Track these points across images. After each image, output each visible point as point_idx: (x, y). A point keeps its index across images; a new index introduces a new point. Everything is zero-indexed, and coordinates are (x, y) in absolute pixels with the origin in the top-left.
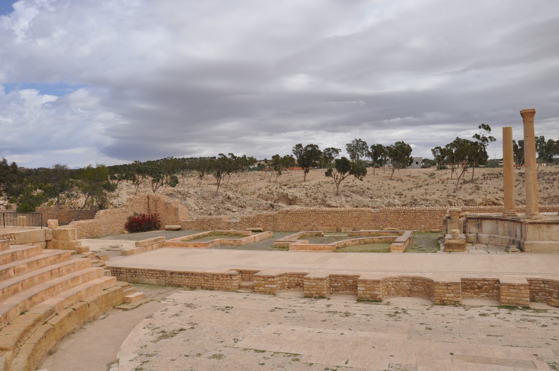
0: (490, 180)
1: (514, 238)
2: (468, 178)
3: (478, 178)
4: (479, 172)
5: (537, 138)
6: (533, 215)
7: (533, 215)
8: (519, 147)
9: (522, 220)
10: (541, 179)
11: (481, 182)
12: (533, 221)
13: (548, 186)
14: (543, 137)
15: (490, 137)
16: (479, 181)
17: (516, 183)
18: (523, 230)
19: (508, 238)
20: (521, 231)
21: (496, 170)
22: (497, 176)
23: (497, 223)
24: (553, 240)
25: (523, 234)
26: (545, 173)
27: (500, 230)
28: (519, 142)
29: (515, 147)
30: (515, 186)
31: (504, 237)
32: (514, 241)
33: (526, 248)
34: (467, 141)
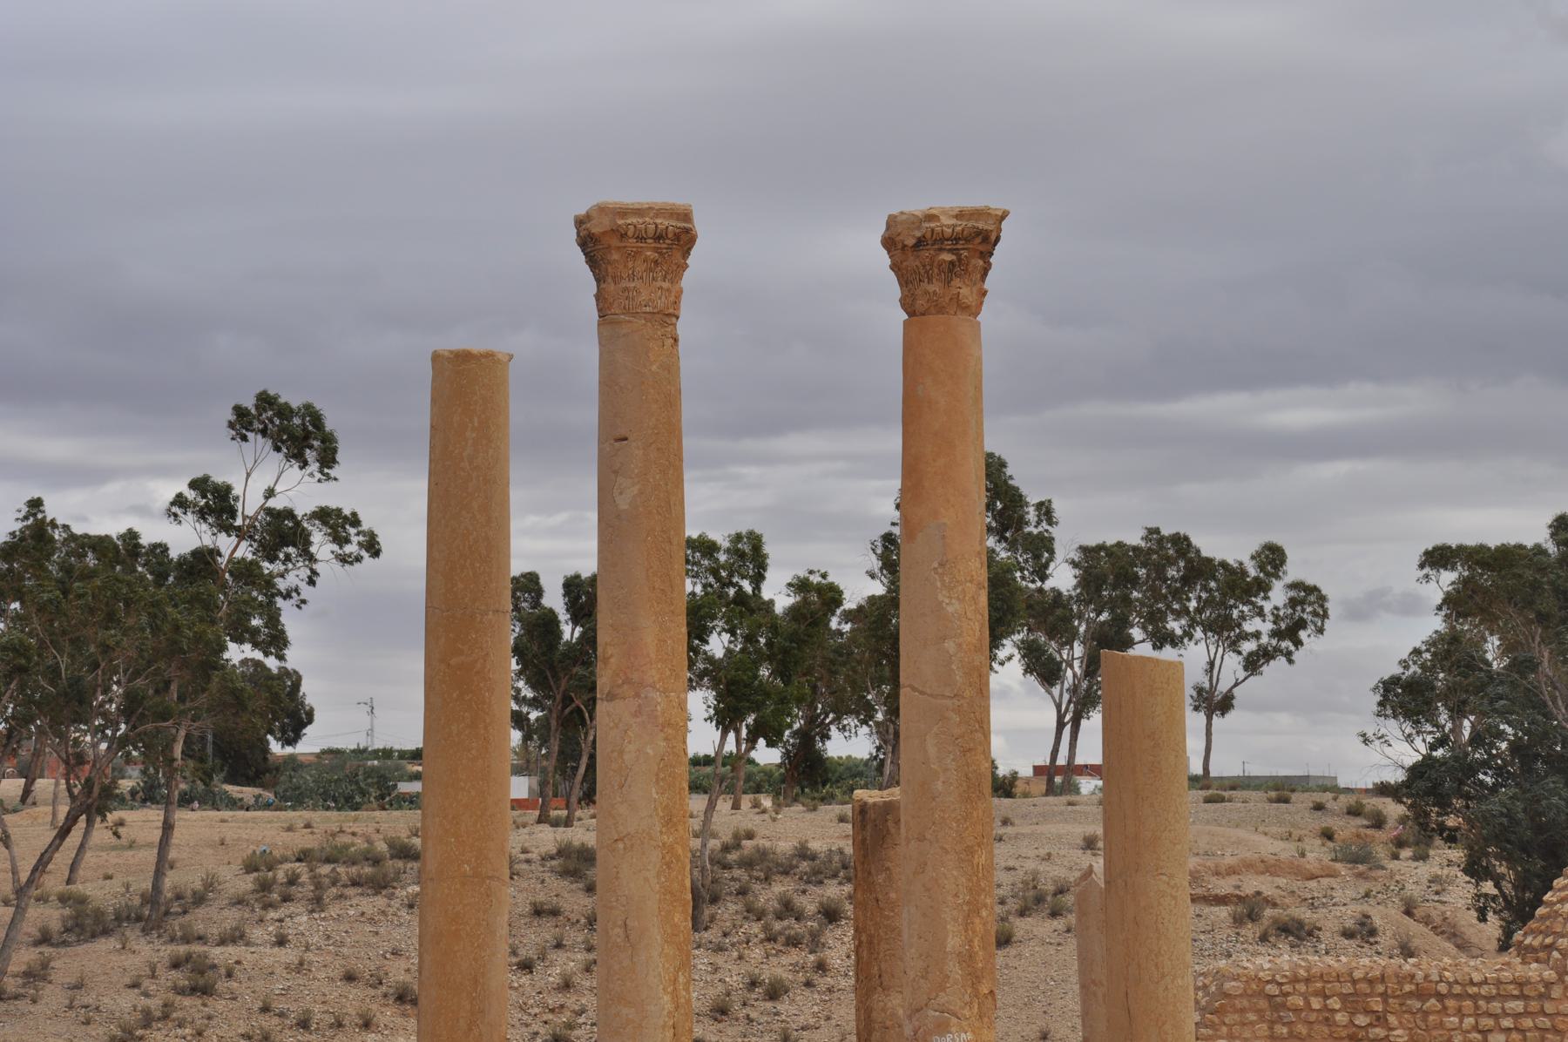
0: (317, 903)
2: (116, 886)
3: (210, 884)
4: (220, 838)
5: (706, 547)
8: (569, 632)
10: (729, 910)
11: (231, 917)
13: (780, 967)
14: (756, 541)
15: (324, 515)
16: (215, 918)
17: (534, 937)
26: (763, 854)
28: (573, 586)
30: (526, 966)
34: (126, 550)
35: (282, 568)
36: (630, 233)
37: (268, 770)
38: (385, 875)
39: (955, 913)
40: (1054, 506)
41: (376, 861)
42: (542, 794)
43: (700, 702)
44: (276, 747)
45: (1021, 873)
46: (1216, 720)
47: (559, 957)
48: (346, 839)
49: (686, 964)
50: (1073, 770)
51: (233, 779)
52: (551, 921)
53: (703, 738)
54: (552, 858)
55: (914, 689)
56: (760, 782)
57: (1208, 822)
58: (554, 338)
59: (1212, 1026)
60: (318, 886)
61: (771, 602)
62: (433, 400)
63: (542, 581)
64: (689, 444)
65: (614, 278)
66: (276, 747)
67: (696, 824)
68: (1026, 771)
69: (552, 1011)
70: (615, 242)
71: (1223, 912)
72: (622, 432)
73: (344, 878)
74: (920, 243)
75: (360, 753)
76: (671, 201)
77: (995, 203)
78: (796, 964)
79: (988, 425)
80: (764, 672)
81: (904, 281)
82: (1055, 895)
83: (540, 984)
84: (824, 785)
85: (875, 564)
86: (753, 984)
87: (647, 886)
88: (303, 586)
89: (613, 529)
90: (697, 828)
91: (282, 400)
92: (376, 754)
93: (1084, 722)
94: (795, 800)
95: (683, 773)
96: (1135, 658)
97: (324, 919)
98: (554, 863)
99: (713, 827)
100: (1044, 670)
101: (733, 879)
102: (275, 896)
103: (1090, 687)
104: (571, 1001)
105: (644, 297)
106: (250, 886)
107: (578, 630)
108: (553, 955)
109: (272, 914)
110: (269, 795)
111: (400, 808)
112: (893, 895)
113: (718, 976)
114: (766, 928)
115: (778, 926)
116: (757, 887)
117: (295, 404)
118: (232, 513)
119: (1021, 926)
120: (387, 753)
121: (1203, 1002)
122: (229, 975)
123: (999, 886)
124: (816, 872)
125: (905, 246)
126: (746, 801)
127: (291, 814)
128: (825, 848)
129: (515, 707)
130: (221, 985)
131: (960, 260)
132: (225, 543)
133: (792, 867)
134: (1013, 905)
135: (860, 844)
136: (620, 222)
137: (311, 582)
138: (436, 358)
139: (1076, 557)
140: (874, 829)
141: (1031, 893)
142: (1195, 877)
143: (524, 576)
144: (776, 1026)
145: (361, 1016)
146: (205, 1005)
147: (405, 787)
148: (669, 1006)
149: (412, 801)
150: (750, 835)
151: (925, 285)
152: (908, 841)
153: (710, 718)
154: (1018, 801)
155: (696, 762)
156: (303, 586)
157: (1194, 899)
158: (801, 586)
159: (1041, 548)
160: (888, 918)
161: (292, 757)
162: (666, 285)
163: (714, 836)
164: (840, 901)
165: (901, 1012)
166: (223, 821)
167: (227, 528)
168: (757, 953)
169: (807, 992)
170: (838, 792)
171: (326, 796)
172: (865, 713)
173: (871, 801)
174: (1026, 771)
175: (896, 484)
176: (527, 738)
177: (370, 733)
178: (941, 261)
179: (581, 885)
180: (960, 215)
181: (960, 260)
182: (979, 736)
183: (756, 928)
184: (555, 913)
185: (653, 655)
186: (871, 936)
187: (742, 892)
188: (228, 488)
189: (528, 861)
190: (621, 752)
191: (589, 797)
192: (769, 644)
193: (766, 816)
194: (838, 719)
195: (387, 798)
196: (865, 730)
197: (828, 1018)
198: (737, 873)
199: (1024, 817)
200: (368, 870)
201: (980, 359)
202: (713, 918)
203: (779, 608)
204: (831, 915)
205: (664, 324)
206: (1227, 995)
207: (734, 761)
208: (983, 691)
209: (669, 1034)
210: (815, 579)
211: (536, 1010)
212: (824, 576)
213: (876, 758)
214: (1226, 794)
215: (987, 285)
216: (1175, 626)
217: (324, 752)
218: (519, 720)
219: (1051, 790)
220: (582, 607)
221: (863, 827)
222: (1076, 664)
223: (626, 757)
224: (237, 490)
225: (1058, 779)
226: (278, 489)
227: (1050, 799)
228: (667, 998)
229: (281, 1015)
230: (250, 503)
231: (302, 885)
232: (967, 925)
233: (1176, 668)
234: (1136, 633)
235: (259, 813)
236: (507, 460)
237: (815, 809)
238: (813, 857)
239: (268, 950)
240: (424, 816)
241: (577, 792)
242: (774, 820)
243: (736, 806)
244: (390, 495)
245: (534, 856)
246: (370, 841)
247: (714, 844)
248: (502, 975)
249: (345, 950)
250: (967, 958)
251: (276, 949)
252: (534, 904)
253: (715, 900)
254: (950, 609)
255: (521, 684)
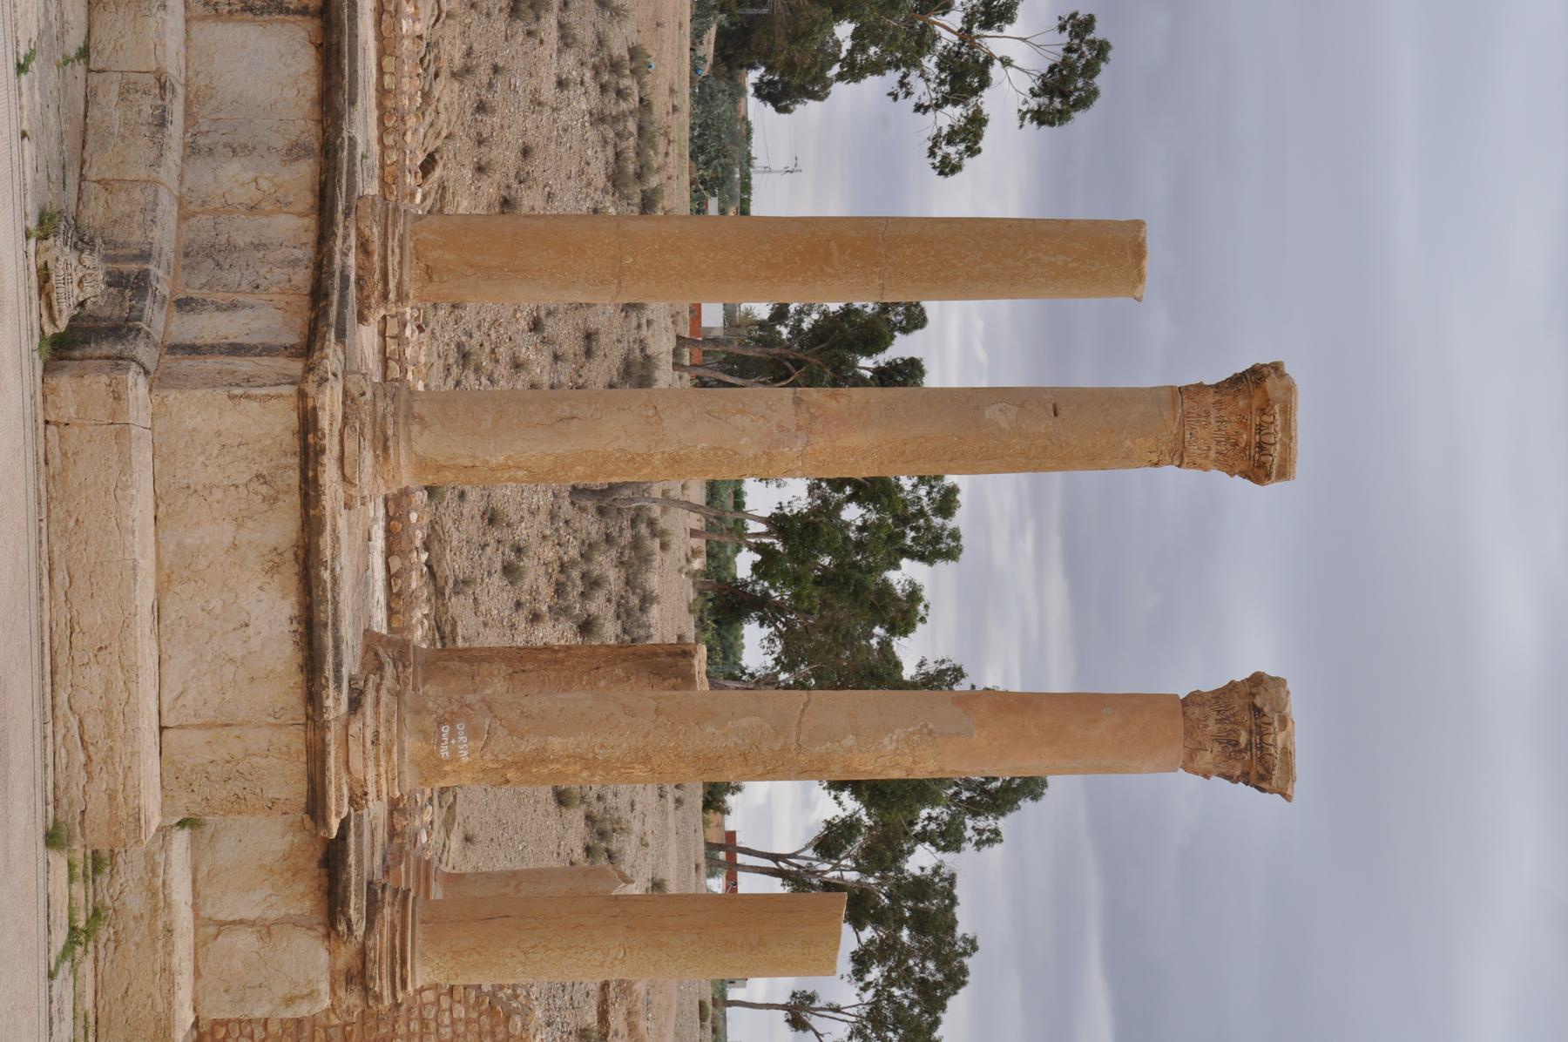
0: (599, 119)
1: (164, 289)
6: (383, 447)
7: (383, 447)
8: (866, 364)
9: (332, 356)
10: (591, 526)
11: (586, 35)
12: (331, 445)
13: (535, 577)
14: (952, 555)
15: (976, 123)
17: (564, 332)
18: (244, 365)
19: (165, 236)
20: (236, 349)
21: (674, 175)
22: (627, 177)
23: (295, 152)
24: (160, 591)
25: (211, 364)
26: (646, 559)
27: (233, 178)
28: (909, 371)
29: (873, 335)
30: (536, 326)
31: (168, 210)
32: (139, 285)
33: (80, 389)
35: (932, 77)
36: (1265, 418)
37: (730, 69)
38: (626, 185)
39: (585, 745)
40: (996, 845)
41: (640, 176)
42: (706, 340)
43: (794, 494)
44: (753, 77)
45: (629, 816)
46: (782, 1014)
47: (545, 358)
48: (662, 147)
49: (535, 477)
50: (732, 869)
51: (721, 34)
52: (580, 350)
53: (762, 499)
54: (642, 350)
55: (806, 704)
56: (718, 559)
57: (680, 1004)
58: (1161, 343)
59: (478, 1003)
60: (616, 120)
61: (897, 567)
62: (1095, 223)
63: (918, 333)
64: (1056, 479)
65: (1220, 402)
66: (753, 77)
67: (675, 493)
68: (730, 823)
69: (493, 351)
70: (1256, 403)
71: (591, 1018)
72: (1063, 411)
73: (623, 145)
74: (1257, 711)
75: (748, 159)
76: (1299, 459)
77: (1299, 788)
78: (538, 593)
79: (1077, 780)
80: (826, 560)
81: (1218, 695)
82: (607, 850)
83: (518, 339)
84: (715, 622)
85: (931, 668)
86: (519, 550)
87: (612, 440)
88: (913, 100)
89: (967, 402)
90: (672, 494)
91: (1103, 65)
92: (746, 177)
93: (779, 881)
94: (701, 593)
95: (725, 474)
96: (839, 927)
97: (583, 125)
98: (638, 352)
99: (673, 510)
100: (831, 841)
101: (621, 530)
102: (606, 77)
103: (813, 887)
104: (503, 370)
105: (1200, 432)
106: (616, 53)
107: (868, 374)
108: (547, 352)
109: (588, 75)
110: (705, 70)
111: (693, 200)
112: (602, 684)
113: (527, 515)
114: (573, 563)
115: (575, 574)
116: (614, 553)
117: (1098, 81)
118: (987, 25)
119: (576, 815)
120: (746, 187)
121: (501, 994)
122: (530, 34)
123: (616, 795)
124: (629, 613)
125: (1254, 695)
126: (699, 543)
127: (687, 92)
128: (652, 621)
129: (792, 309)
130: (519, 26)
131: (1240, 751)
132: (954, 19)
133: (633, 589)
134: (597, 809)
135: (653, 652)
136: (1277, 408)
137: (919, 108)
138: (1138, 225)
139: (945, 871)
140: (668, 664)
141: (608, 827)
142: (625, 988)
143: (922, 311)
144: (477, 573)
145: (489, 163)
146: (501, 10)
147: (713, 206)
148: (493, 462)
149: (700, 210)
150: (664, 546)
151: (1214, 716)
152: (656, 698)
153: (781, 508)
154: (700, 814)
155: (738, 494)
156: (913, 100)
157: (605, 986)
158: (914, 595)
159: (949, 839)
160: (580, 679)
161: (743, 91)
162: (1212, 454)
163: (664, 511)
164: (600, 636)
165: (489, 691)
166: (680, 25)
167: (969, 19)
168: (549, 554)
169: (510, 604)
170: (708, 635)
171: (705, 126)
172: (788, 661)
173: (696, 662)
174: (730, 823)
175: (1016, 687)
176: (762, 325)
177: (768, 170)
178: (1240, 732)
179: (615, 379)
180: (1287, 752)
181: (1240, 751)
182: (760, 769)
183: (573, 552)
184: (589, 353)
185: (838, 443)
186: (562, 662)
187: (609, 539)
188: (1011, 20)
189: (639, 326)
190: (742, 412)
191: (702, 383)
192: (854, 565)
193: (683, 562)
194: (781, 635)
195: (703, 187)
196: (770, 662)
197: (485, 625)
198: (628, 534)
199: (684, 821)
200: (631, 168)
201: (1139, 771)
202: (583, 510)
203: (893, 576)
204: (587, 627)
205: (1172, 452)
206: (508, 1018)
207: (738, 529)
208: (803, 773)
209: (467, 462)
210: (921, 608)
211: (493, 336)
212: (922, 620)
213: (743, 673)
214: (708, 1023)
215: (1215, 779)
216: (875, 974)
217: (748, 124)
218: (780, 314)
219: (711, 847)
220: (891, 377)
221: (670, 654)
222: (836, 874)
223: (737, 417)
224: (1009, 30)
225: (722, 855)
226: (1011, 71)
227: (702, 847)
228: (501, 459)
229: (490, 85)
230: (995, 43)
231: (617, 103)
232: (574, 757)
233: (829, 968)
234: (868, 933)
235: (688, 61)
236: (1034, 296)
237: (691, 611)
238: (643, 609)
239: (553, 71)
240: (682, 217)
241: (707, 374)
242: (680, 571)
243: (694, 533)
244: (1004, 179)
245: (644, 332)
246: (658, 170)
247: (656, 511)
248: (529, 298)
249: (553, 146)
250: (540, 757)
251: (554, 79)
252: (597, 332)
253: (601, 512)
254: (886, 741)
255: (815, 316)
